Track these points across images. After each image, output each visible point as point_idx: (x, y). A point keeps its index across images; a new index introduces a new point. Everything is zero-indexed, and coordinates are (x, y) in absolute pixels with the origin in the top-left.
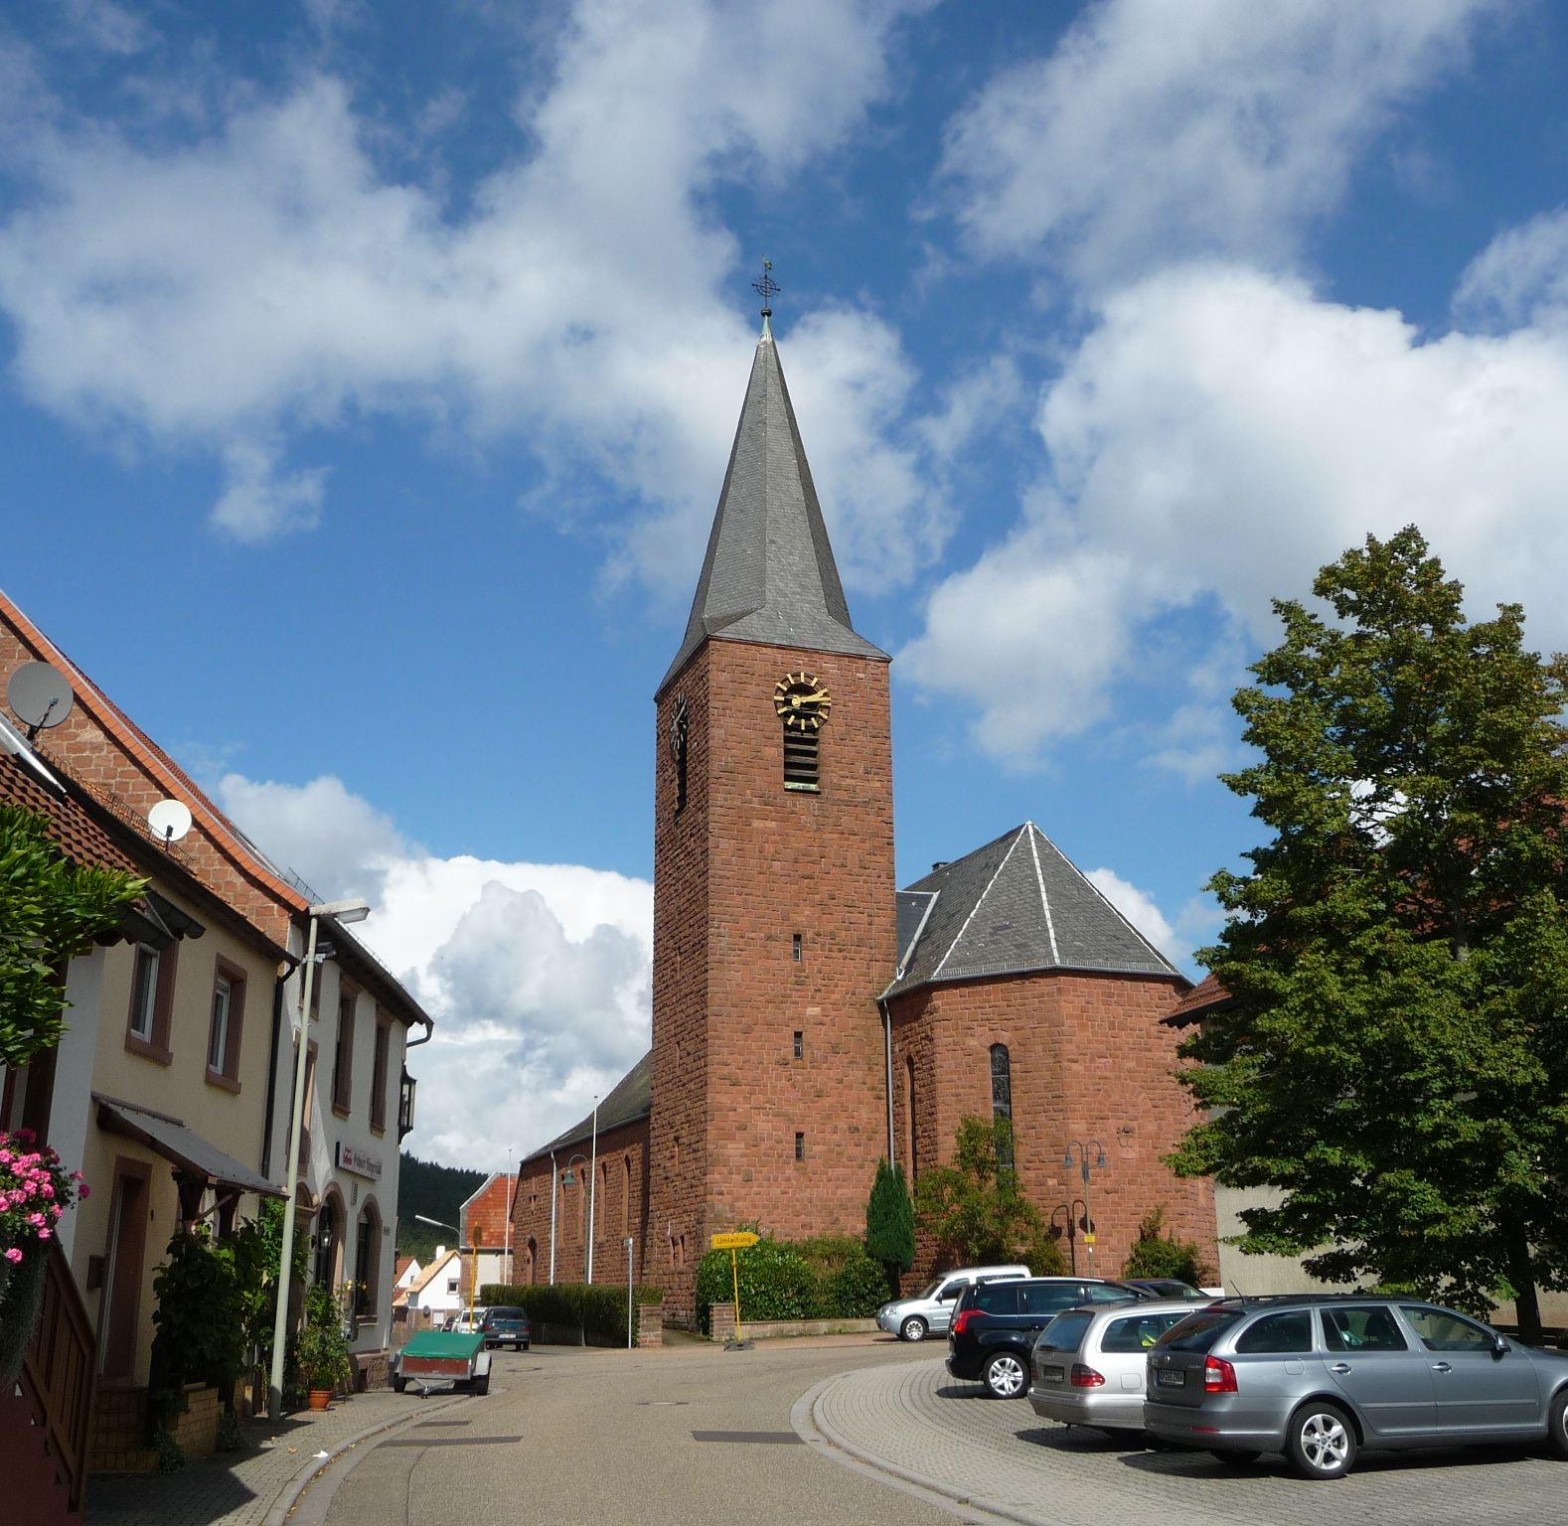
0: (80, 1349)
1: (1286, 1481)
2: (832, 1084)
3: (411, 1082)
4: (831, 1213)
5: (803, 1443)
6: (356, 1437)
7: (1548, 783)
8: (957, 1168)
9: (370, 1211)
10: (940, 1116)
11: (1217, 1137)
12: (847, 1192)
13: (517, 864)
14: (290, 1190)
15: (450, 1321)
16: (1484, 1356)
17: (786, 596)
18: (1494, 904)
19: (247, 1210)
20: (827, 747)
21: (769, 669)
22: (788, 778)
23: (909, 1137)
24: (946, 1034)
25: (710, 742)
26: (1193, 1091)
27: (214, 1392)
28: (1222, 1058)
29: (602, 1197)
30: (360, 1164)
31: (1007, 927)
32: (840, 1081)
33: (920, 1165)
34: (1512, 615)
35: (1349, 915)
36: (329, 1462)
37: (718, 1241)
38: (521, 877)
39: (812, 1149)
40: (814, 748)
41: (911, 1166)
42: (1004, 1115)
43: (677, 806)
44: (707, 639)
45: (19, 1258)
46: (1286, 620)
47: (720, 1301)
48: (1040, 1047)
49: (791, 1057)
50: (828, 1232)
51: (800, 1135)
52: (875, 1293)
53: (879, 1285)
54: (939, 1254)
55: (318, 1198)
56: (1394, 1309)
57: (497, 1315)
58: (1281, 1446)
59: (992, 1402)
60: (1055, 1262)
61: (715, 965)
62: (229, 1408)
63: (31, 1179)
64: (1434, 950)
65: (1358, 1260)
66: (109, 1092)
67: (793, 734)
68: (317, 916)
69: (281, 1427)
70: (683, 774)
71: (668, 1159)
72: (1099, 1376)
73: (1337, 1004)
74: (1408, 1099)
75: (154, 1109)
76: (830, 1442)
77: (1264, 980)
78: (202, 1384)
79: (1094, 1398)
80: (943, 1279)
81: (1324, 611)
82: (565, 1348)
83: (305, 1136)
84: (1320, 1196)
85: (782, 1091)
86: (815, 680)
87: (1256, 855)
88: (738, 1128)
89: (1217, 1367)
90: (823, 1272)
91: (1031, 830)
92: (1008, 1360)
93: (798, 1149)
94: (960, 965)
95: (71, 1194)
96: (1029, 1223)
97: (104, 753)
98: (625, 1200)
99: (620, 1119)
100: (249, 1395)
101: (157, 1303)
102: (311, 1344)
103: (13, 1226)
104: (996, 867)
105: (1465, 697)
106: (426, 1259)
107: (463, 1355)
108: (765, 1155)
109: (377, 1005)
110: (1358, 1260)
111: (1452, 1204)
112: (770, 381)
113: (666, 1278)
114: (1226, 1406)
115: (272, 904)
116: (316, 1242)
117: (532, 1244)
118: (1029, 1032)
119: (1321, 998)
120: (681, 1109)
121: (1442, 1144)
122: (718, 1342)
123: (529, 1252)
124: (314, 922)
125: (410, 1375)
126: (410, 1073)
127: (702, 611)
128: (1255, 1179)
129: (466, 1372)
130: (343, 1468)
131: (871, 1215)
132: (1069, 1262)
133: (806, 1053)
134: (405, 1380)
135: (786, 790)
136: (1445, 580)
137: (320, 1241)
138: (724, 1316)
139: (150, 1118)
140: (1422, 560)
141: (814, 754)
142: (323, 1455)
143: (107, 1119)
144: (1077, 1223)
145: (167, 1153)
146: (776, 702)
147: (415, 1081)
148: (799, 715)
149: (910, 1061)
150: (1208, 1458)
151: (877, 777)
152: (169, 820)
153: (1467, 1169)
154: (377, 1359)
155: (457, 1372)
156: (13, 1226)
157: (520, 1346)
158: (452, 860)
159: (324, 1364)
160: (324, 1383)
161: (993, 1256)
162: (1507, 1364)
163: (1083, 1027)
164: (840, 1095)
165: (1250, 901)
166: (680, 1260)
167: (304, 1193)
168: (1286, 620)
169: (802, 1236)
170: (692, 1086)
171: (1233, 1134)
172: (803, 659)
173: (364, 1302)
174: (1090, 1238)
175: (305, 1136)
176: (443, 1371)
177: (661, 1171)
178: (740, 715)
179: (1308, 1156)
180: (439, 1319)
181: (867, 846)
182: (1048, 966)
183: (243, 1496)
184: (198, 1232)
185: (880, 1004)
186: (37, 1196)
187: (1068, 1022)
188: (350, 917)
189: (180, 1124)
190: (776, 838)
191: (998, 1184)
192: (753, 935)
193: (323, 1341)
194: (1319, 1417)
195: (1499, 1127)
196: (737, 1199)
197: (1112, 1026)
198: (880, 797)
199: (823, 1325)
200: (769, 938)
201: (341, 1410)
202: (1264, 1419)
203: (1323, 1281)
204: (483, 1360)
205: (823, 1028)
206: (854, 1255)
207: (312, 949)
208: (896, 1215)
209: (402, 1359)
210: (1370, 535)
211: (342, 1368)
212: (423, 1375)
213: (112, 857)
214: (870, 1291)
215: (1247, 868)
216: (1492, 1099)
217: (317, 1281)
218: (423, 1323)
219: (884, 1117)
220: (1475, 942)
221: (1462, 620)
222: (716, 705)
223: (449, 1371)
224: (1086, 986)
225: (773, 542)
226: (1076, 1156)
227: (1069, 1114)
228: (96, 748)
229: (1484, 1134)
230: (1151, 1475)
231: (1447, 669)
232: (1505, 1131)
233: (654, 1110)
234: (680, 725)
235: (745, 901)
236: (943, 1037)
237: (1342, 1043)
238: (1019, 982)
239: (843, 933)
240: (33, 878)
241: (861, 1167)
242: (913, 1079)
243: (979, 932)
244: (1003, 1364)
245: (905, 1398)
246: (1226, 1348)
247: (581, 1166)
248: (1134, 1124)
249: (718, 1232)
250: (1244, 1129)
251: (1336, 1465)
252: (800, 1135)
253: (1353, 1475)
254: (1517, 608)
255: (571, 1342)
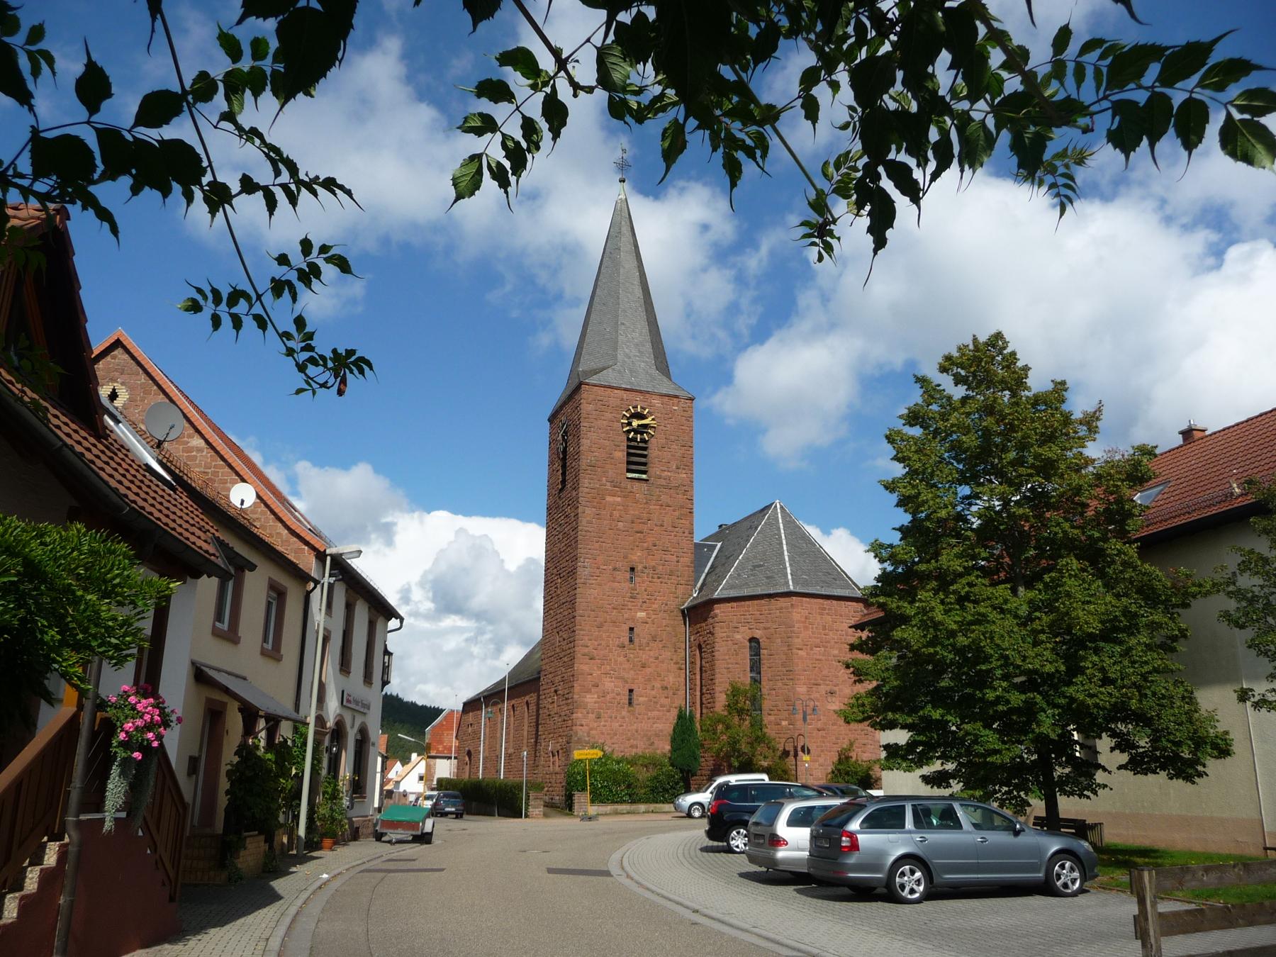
0: (177, 810)
1: (887, 905)
2: (652, 660)
3: (390, 654)
4: (650, 739)
5: (612, 876)
6: (347, 867)
7: (1075, 491)
8: (726, 713)
9: (363, 734)
10: (717, 681)
11: (870, 700)
12: (659, 726)
13: (473, 517)
14: (311, 720)
15: (417, 799)
16: (1009, 834)
17: (630, 358)
18: (1044, 563)
19: (285, 730)
20: (653, 452)
21: (619, 402)
22: (629, 471)
23: (698, 693)
24: (723, 630)
25: (581, 448)
26: (853, 673)
27: (262, 838)
28: (872, 652)
29: (512, 726)
30: (357, 703)
31: (761, 566)
32: (657, 658)
33: (704, 711)
34: (1060, 387)
35: (951, 569)
36: (328, 880)
37: (577, 754)
38: (478, 526)
39: (639, 699)
40: (645, 453)
41: (699, 711)
42: (756, 681)
43: (560, 487)
44: (581, 384)
45: (140, 758)
46: (922, 387)
47: (579, 791)
48: (779, 640)
49: (627, 642)
50: (647, 751)
51: (631, 691)
52: (674, 788)
53: (677, 783)
54: (714, 765)
55: (330, 723)
56: (956, 806)
57: (445, 796)
58: (884, 884)
59: (730, 855)
60: (785, 772)
61: (580, 585)
62: (271, 847)
63: (148, 713)
64: (1002, 591)
65: (953, 775)
66: (200, 659)
67: (633, 444)
68: (330, 555)
69: (303, 860)
70: (564, 467)
71: (551, 704)
72: (784, 840)
73: (941, 623)
74: (983, 680)
75: (229, 669)
76: (628, 876)
77: (898, 607)
78: (257, 832)
79: (781, 854)
80: (715, 781)
81: (946, 382)
82: (488, 817)
83: (322, 687)
84: (927, 737)
85: (621, 664)
86: (647, 410)
87: (901, 529)
88: (593, 686)
89: (848, 836)
90: (643, 775)
91: (778, 506)
92: (742, 830)
93: (630, 699)
94: (731, 589)
95: (172, 721)
96: (769, 748)
97: (204, 453)
98: (526, 728)
99: (524, 678)
100: (285, 840)
101: (229, 784)
102: (323, 811)
103: (137, 740)
104: (756, 528)
105: (1023, 438)
106: (405, 760)
107: (417, 820)
108: (609, 702)
109: (369, 608)
110: (953, 775)
111: (1004, 743)
112: (623, 223)
113: (548, 776)
114: (852, 859)
115: (304, 547)
116: (329, 750)
117: (469, 753)
119: (932, 619)
120: (560, 673)
121: (1000, 708)
122: (578, 816)
123: (467, 759)
124: (329, 558)
125: (385, 831)
126: (390, 649)
127: (578, 365)
128: (891, 725)
129: (418, 830)
130: (336, 884)
131: (673, 740)
132: (794, 772)
133: (636, 640)
134: (382, 835)
135: (628, 478)
136: (1019, 364)
137: (331, 750)
138: (582, 800)
139: (226, 675)
140: (1005, 352)
141: (645, 456)
142: (325, 876)
143: (200, 676)
144: (799, 749)
145: (235, 696)
146: (623, 423)
147: (392, 654)
148: (636, 431)
149: (700, 647)
150: (846, 891)
151: (684, 472)
152: (242, 495)
153: (1016, 723)
154: (365, 821)
155: (413, 830)
156: (137, 740)
157: (458, 815)
158: (433, 513)
159: (332, 823)
160: (333, 835)
161: (747, 767)
162: (1021, 839)
163: (806, 628)
164: (657, 667)
165: (893, 558)
166: (556, 765)
167: (320, 720)
168: (922, 387)
169: (631, 753)
170: (565, 659)
171: (880, 698)
172: (639, 397)
173: (359, 787)
174: (806, 758)
175: (322, 687)
176: (404, 829)
177: (546, 711)
178: (600, 431)
179: (921, 713)
180: (412, 798)
181: (677, 513)
182: (786, 590)
183: (275, 897)
184: (253, 743)
185: (683, 611)
186: (151, 722)
187: (797, 625)
188: (351, 556)
189: (245, 679)
190: (621, 508)
191: (750, 723)
192: (605, 567)
193: (331, 809)
194: (907, 867)
195: (1034, 698)
196: (591, 729)
197: (824, 628)
198: (685, 483)
199: (642, 807)
200: (615, 569)
201: (341, 851)
202: (875, 868)
203: (932, 787)
204: (429, 823)
205: (647, 625)
206: (662, 765)
207: (327, 574)
208: (688, 741)
209: (380, 822)
210: (974, 336)
211: (343, 826)
212: (392, 831)
213: (202, 523)
214: (672, 787)
215: (895, 538)
216: (1034, 682)
217: (329, 773)
218: (403, 801)
219: (683, 680)
220: (1029, 586)
221: (1029, 389)
222: (585, 424)
223: (409, 829)
224: (809, 603)
225: (623, 324)
226: (799, 706)
227: (797, 682)
228: (199, 450)
229: (1025, 702)
230: (809, 899)
231: (1013, 419)
232: (1038, 701)
233: (543, 673)
234: (563, 436)
235: (601, 547)
236: (720, 633)
237: (943, 646)
239: (661, 567)
241: (669, 711)
242: (701, 658)
243: (744, 569)
244: (738, 833)
245: (680, 851)
246: (854, 826)
247: (499, 706)
248: (836, 689)
249: (579, 749)
250: (887, 695)
251: (917, 895)
252: (631, 691)
253: (927, 902)
254: (1063, 383)
255: (491, 814)
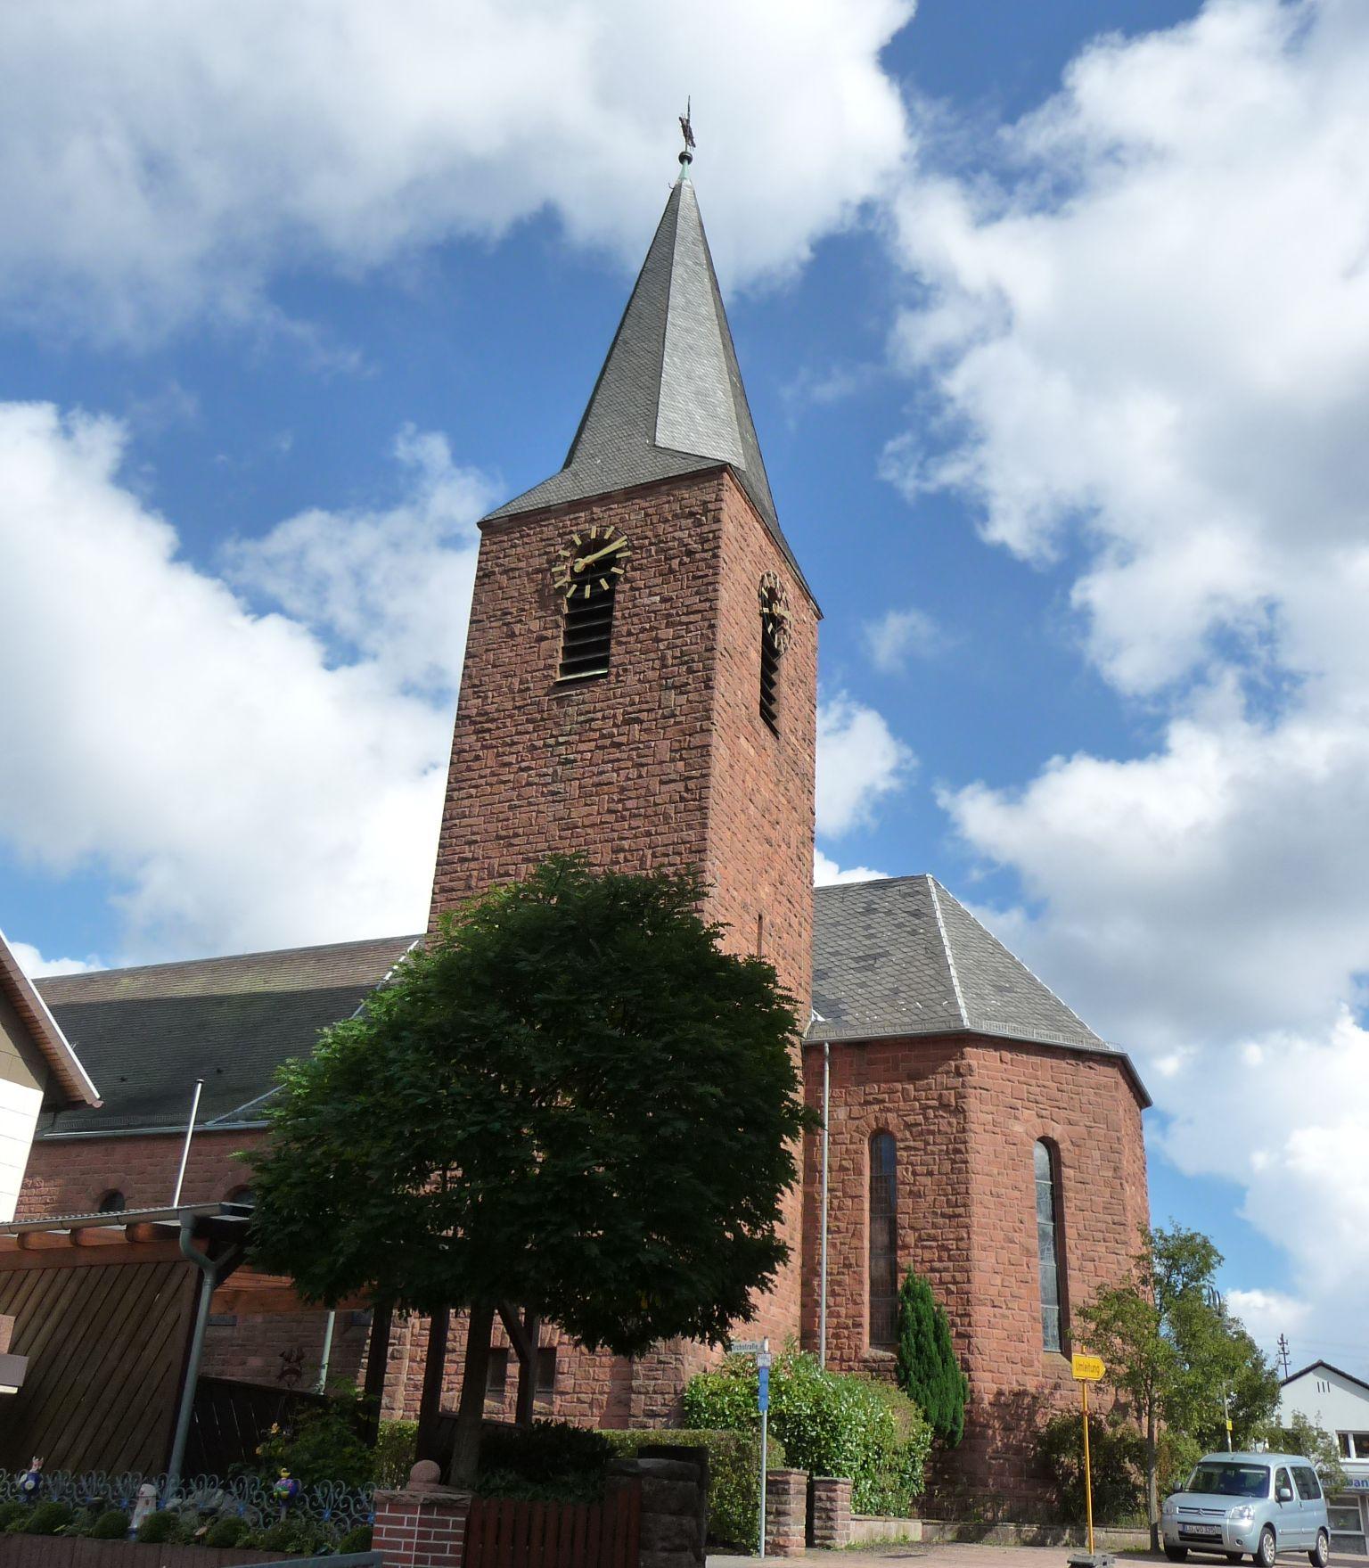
118: (1083, 1130)
238: (1073, 1062)
240: (454, 1058)
